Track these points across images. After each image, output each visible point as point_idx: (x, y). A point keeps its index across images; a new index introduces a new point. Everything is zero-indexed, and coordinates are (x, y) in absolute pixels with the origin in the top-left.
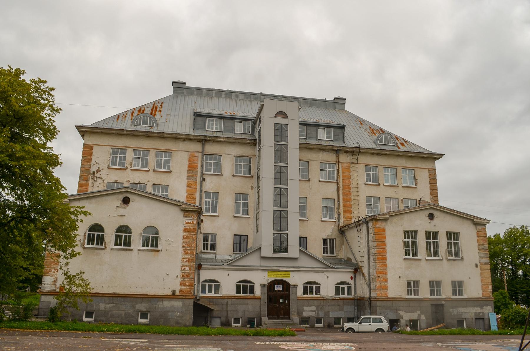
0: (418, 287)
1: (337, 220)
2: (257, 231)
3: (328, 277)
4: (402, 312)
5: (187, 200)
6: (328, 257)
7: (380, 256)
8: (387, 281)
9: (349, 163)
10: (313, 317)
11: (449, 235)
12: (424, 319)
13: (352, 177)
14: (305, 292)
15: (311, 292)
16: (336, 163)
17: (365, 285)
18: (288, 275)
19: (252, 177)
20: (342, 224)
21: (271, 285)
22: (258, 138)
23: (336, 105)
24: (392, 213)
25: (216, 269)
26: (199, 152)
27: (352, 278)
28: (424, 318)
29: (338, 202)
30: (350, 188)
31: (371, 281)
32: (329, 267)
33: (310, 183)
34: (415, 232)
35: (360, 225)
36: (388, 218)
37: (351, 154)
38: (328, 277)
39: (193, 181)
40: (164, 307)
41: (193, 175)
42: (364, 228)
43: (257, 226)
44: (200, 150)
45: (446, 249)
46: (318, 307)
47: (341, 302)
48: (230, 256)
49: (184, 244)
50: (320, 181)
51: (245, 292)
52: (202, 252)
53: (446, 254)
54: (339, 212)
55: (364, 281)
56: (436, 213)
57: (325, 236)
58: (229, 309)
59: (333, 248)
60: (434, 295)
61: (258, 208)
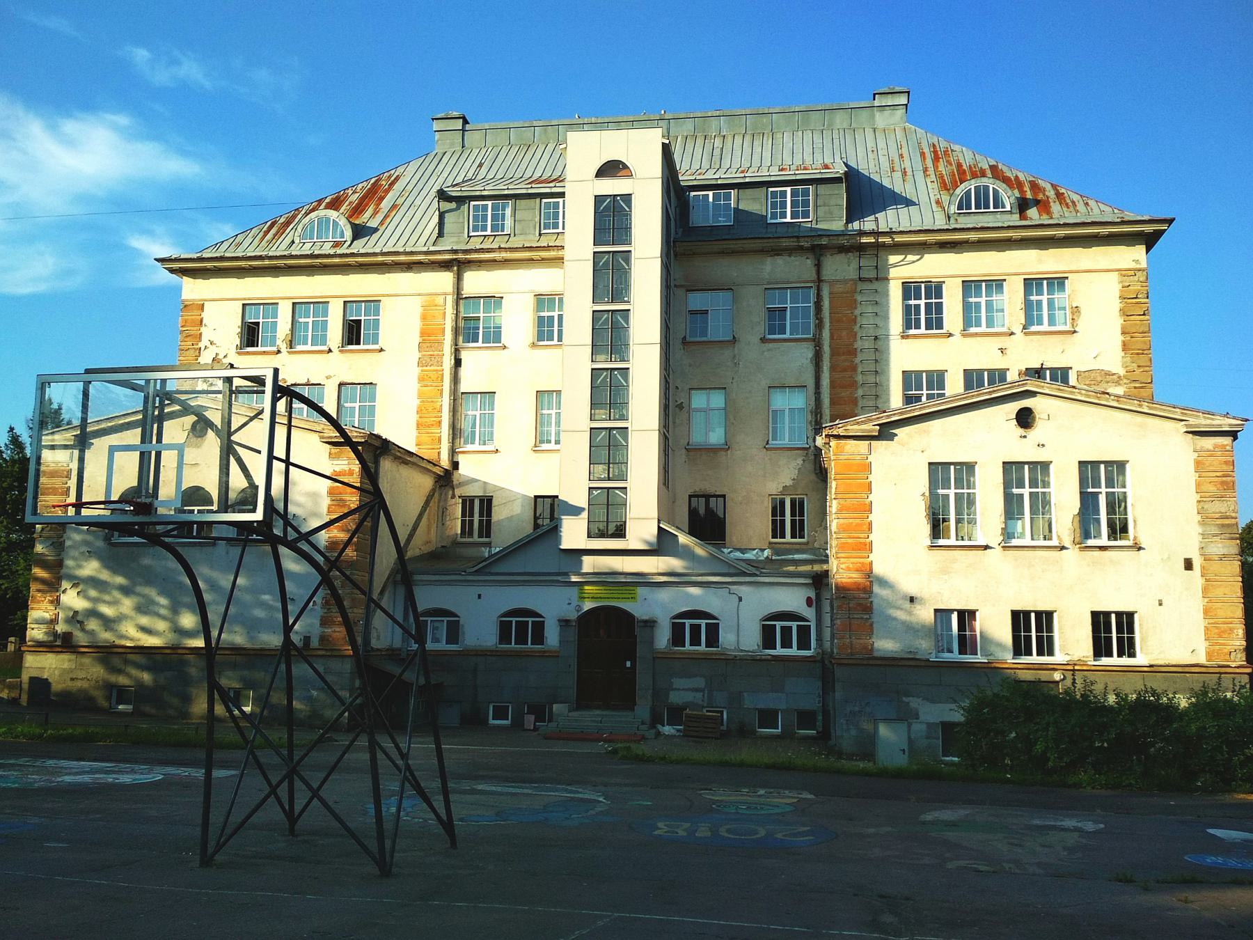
3: (740, 599)
4: (915, 698)
5: (420, 417)
7: (850, 541)
11: (1088, 470)
15: (695, 641)
16: (812, 285)
18: (632, 596)
27: (809, 602)
30: (853, 352)
33: (736, 349)
34: (970, 467)
38: (740, 599)
39: (432, 368)
41: (432, 353)
52: (456, 544)
59: (802, 522)
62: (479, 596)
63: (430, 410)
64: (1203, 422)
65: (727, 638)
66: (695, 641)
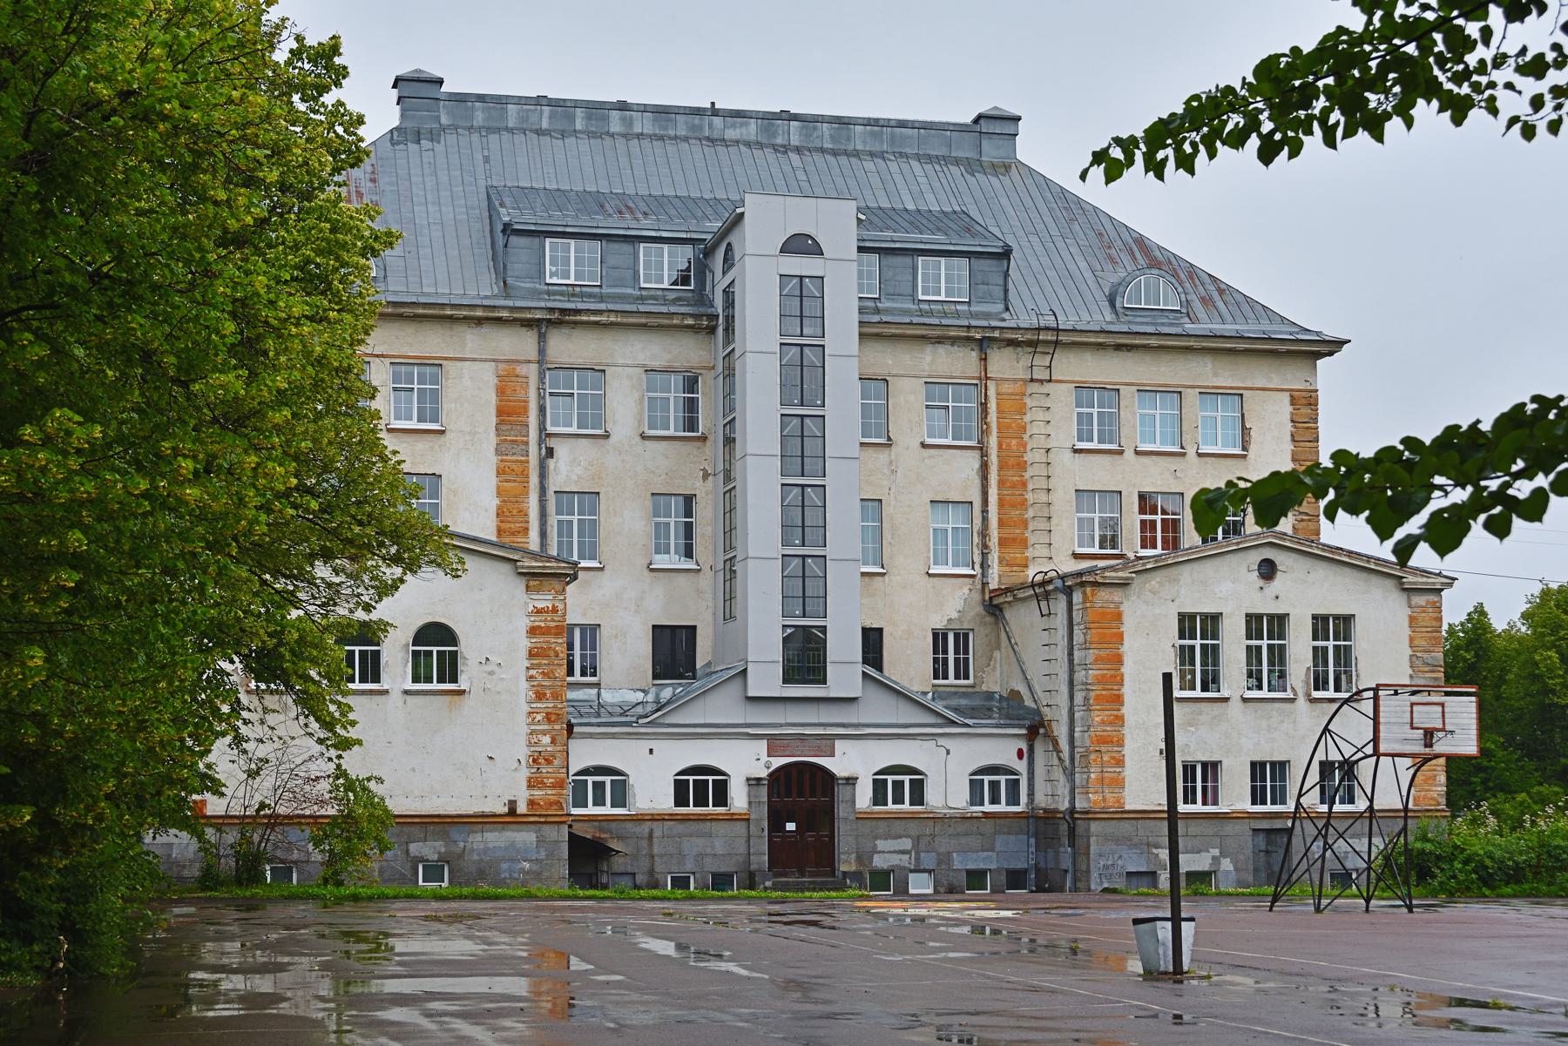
0: (1215, 780)
1: (980, 571)
2: (729, 616)
3: (948, 752)
6: (948, 689)
8: (1123, 762)
9: (1022, 380)
10: (905, 868)
11: (1320, 625)
12: (1230, 871)
13: (1032, 429)
14: (879, 796)
15: (898, 799)
17: (1058, 774)
19: (704, 439)
20: (993, 585)
21: (779, 779)
22: (720, 311)
23: (984, 142)
24: (1144, 564)
25: (613, 736)
26: (529, 362)
27: (1020, 754)
28: (1231, 868)
29: (985, 511)
30: (1022, 466)
31: (1076, 764)
32: (953, 723)
35: (1047, 595)
36: (1132, 579)
37: (1030, 349)
38: (948, 752)
39: (514, 458)
40: (488, 849)
42: (1060, 605)
43: (730, 598)
44: (534, 355)
45: (1309, 668)
46: (917, 841)
47: (988, 826)
48: (643, 691)
49: (533, 672)
50: (924, 445)
51: (701, 801)
53: (1308, 684)
54: (985, 546)
55: (1056, 762)
56: (1280, 558)
57: (940, 624)
58: (656, 850)
59: (966, 661)
60: (1264, 802)
61: (729, 546)
62: (651, 751)
63: (515, 512)
64: (1421, 580)
65: (934, 798)
66: (898, 799)
